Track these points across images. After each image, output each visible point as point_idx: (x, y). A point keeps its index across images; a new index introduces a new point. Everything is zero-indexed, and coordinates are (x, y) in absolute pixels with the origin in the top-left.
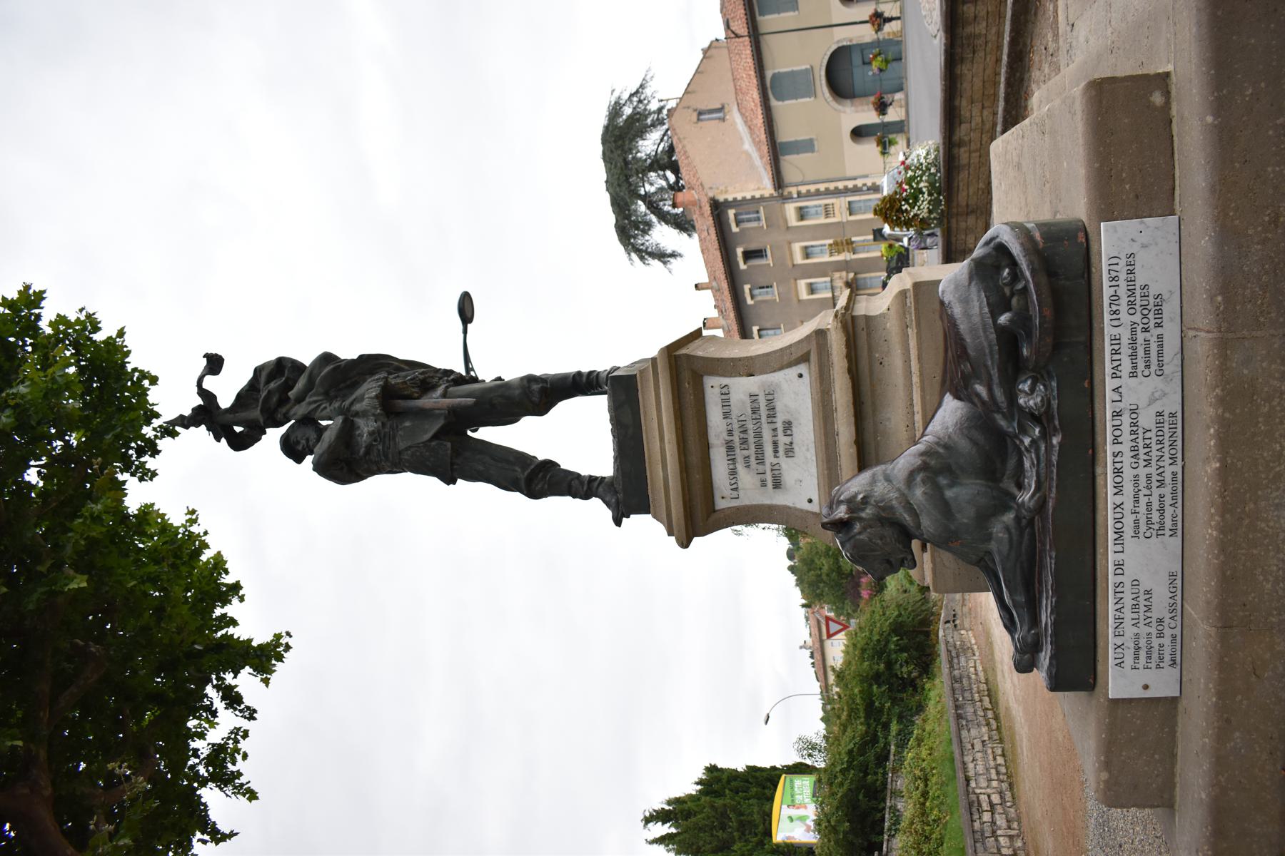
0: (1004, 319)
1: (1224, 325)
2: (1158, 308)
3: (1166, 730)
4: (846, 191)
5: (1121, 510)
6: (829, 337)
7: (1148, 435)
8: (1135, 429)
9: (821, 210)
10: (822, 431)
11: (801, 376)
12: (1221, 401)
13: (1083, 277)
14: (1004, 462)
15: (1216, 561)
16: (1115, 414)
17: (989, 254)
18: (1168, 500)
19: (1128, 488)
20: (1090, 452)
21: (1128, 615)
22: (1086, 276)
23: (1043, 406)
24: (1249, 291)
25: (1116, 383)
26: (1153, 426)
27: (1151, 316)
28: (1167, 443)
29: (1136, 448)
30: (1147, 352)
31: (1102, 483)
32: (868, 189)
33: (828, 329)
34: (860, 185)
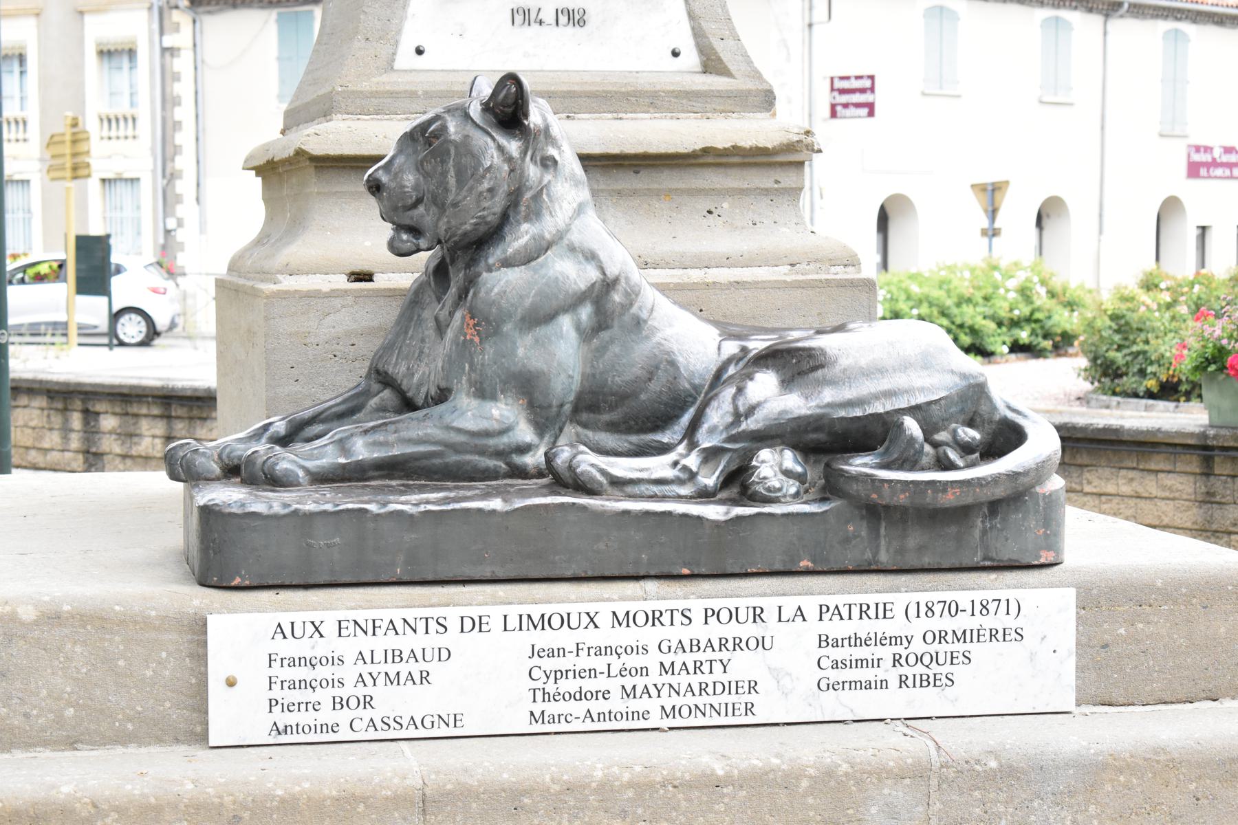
0: (912, 426)
1: (951, 773)
2: (931, 680)
3: (130, 726)
4: (170, 176)
5: (583, 624)
6: (758, 115)
7: (717, 667)
8: (730, 645)
9: (123, 108)
10: (576, 88)
11: (675, 54)
12: (829, 774)
13: (985, 559)
14: (613, 427)
15: (548, 778)
16: (758, 611)
17: (995, 408)
18: (597, 706)
19: (625, 636)
20: (686, 571)
21: (382, 642)
22: (987, 563)
23: (769, 490)
24: (1002, 809)
25: (811, 612)
26: (732, 675)
27: (920, 669)
28: (701, 701)
29: (695, 648)
30: (861, 663)
31: (629, 592)
32: (168, 232)
33: (774, 115)
34: (180, 210)
